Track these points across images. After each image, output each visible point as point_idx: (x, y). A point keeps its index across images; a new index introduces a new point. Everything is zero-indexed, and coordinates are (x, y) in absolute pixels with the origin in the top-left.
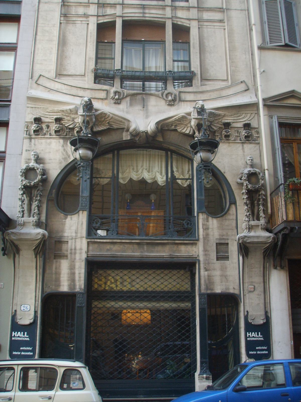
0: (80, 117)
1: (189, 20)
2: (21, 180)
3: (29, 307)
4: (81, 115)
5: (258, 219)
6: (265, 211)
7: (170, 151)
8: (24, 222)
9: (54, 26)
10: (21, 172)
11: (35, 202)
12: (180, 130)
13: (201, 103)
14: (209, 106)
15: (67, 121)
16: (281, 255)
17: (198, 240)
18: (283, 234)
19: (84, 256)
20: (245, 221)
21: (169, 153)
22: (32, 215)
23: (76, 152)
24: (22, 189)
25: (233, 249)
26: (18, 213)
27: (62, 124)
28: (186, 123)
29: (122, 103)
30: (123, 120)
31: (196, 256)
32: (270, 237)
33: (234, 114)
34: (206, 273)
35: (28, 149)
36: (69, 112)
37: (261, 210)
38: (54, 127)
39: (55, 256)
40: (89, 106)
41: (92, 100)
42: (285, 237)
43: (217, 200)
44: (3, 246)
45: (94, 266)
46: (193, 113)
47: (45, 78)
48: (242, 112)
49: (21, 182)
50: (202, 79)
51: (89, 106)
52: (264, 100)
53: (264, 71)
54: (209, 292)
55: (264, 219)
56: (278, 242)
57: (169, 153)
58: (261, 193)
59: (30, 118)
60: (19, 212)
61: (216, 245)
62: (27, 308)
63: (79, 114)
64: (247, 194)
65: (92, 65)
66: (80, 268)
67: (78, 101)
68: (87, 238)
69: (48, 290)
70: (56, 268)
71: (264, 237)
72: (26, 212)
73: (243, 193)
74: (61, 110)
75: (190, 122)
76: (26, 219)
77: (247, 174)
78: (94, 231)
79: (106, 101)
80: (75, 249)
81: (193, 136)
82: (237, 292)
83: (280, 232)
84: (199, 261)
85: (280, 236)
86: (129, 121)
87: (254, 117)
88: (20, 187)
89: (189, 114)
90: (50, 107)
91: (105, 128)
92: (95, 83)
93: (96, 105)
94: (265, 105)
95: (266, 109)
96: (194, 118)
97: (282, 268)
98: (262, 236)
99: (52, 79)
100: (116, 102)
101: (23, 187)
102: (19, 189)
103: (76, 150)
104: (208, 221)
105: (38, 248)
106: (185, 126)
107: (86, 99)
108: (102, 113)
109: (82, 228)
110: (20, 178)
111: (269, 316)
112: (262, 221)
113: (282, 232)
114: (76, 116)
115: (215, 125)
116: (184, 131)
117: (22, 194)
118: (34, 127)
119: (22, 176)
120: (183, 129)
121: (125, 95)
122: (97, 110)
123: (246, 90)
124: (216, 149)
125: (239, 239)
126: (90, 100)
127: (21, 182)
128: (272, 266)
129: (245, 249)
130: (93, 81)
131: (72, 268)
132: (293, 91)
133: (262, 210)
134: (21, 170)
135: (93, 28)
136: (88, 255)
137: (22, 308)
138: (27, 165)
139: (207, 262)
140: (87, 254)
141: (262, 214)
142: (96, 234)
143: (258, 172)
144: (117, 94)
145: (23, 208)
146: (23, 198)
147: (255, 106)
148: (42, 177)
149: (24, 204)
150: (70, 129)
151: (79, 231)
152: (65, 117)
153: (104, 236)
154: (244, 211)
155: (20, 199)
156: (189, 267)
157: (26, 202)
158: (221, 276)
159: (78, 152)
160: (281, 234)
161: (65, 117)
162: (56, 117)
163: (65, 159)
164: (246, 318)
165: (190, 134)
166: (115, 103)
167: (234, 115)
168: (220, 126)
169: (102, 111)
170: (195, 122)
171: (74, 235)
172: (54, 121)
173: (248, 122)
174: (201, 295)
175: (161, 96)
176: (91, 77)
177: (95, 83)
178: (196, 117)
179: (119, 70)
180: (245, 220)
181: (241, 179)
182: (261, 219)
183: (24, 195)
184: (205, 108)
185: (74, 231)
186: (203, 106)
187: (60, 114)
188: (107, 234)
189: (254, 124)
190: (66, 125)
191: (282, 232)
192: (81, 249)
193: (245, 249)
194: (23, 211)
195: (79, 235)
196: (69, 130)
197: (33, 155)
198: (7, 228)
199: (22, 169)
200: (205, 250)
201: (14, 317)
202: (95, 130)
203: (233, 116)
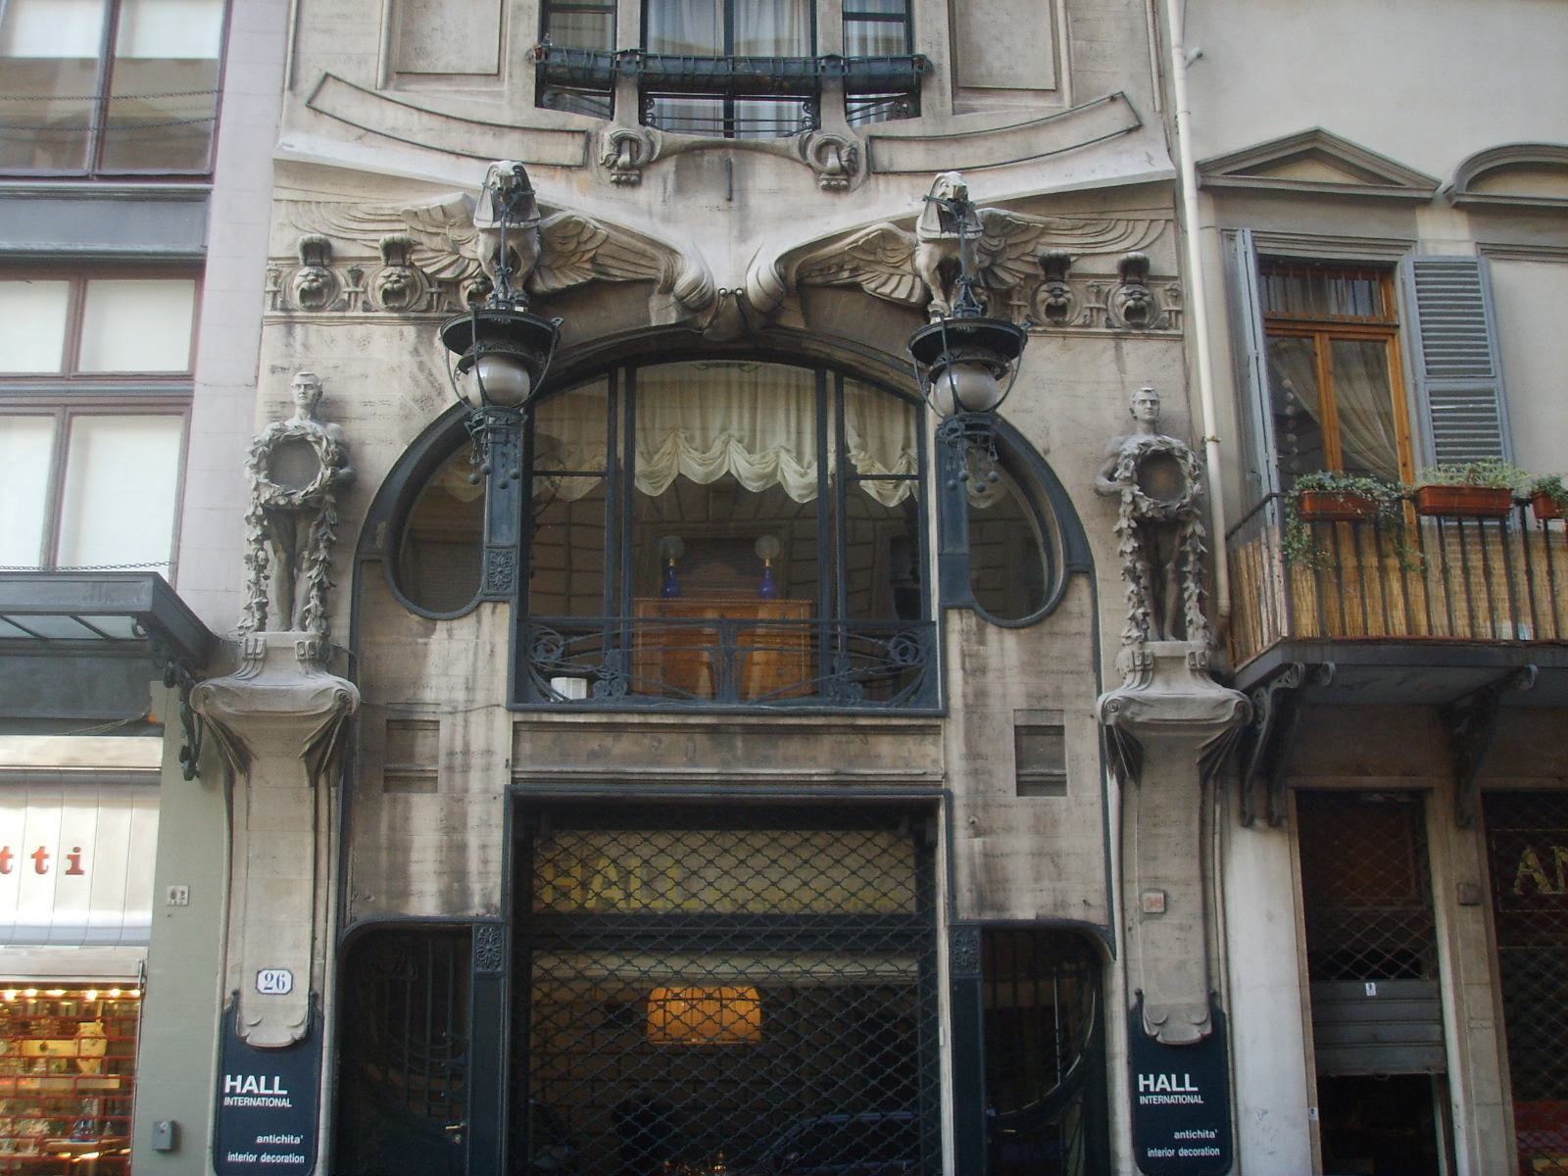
0: (482, 237)
2: (254, 484)
3: (287, 979)
4: (483, 230)
5: (1180, 633)
6: (1206, 603)
7: (832, 369)
8: (267, 650)
10: (253, 453)
11: (310, 569)
12: (873, 286)
13: (953, 179)
15: (430, 254)
16: (1271, 772)
17: (944, 715)
18: (1277, 692)
19: (501, 778)
20: (1129, 642)
21: (830, 376)
22: (296, 619)
23: (467, 373)
24: (260, 520)
25: (1083, 749)
26: (244, 614)
27: (412, 265)
29: (644, 182)
30: (648, 249)
31: (939, 778)
32: (1225, 703)
33: (1082, 223)
34: (978, 842)
36: (440, 217)
37: (1190, 596)
38: (380, 276)
39: (387, 779)
40: (515, 196)
41: (528, 170)
42: (1286, 701)
43: (1019, 560)
44: (185, 742)
45: (540, 819)
47: (343, 87)
49: (255, 494)
50: (957, 88)
51: (515, 196)
52: (1201, 168)
53: (1200, 56)
54: (989, 916)
55: (1201, 632)
56: (1256, 721)
57: (830, 376)
58: (1190, 530)
59: (287, 242)
60: (248, 608)
61: (1017, 734)
62: (281, 984)
63: (478, 225)
64: (1135, 533)
66: (486, 824)
67: (473, 177)
68: (511, 710)
69: (362, 913)
70: (392, 828)
71: (1203, 702)
72: (273, 608)
73: (1120, 532)
74: (406, 212)
76: (273, 634)
78: (540, 680)
79: (583, 175)
80: (466, 752)
81: (921, 311)
82: (1097, 917)
83: (1264, 682)
84: (949, 796)
85: (1267, 699)
86: (672, 252)
87: (1162, 234)
88: (250, 512)
89: (908, 224)
90: (363, 200)
92: (539, 103)
93: (546, 189)
94: (1203, 189)
95: (1209, 202)
96: (927, 241)
97: (1274, 823)
98: (1193, 701)
99: (374, 91)
101: (260, 511)
102: (248, 519)
103: (465, 366)
104: (982, 641)
105: (321, 750)
106: (891, 270)
107: (506, 167)
108: (567, 223)
109: (493, 672)
110: (250, 477)
111: (1225, 1010)
112: (1196, 642)
113: (1275, 685)
114: (466, 234)
115: (1010, 265)
116: (887, 290)
117: (259, 541)
118: (301, 277)
119: (256, 467)
120: (884, 284)
122: (546, 211)
123: (1129, 131)
124: (1015, 361)
125: (1105, 712)
126: (520, 171)
127: (255, 494)
128: (1234, 814)
129: (1128, 748)
130: (533, 99)
131: (454, 826)
132: (1315, 134)
133: (1195, 598)
134: (255, 444)
136: (517, 776)
137: (262, 984)
138: (276, 425)
139: (982, 802)
140: (513, 772)
141: (1193, 613)
142: (546, 694)
143: (1180, 450)
144: (626, 145)
145: (263, 593)
146: (261, 554)
147: (1164, 190)
148: (333, 474)
149: (267, 578)
150: (441, 283)
151: (481, 683)
152: (424, 239)
153: (579, 701)
154: (1125, 601)
155: (248, 559)
156: (909, 819)
157: (274, 570)
158: (1038, 854)
159: (473, 374)
160: (1270, 693)
161: (424, 239)
162: (388, 236)
163: (424, 401)
164: (1134, 1018)
166: (618, 183)
168: (1029, 270)
169: (569, 213)
171: (460, 696)
172: (381, 254)
173: (1140, 254)
174: (957, 929)
175: (796, 154)
176: (524, 80)
177: (539, 103)
178: (937, 235)
179: (634, 52)
180: (1129, 637)
181: (1111, 478)
182: (1190, 631)
183: (268, 545)
184: (971, 199)
185: (460, 683)
186: (961, 191)
187: (403, 226)
188: (590, 694)
189: (1162, 262)
190: (428, 270)
191: (1275, 685)
192: (489, 752)
193: (1128, 748)
194: (262, 606)
195: (480, 697)
196: (440, 290)
197: (299, 386)
198: (199, 673)
199: (259, 441)
200: (973, 754)
201: (229, 1019)
203: (1080, 232)
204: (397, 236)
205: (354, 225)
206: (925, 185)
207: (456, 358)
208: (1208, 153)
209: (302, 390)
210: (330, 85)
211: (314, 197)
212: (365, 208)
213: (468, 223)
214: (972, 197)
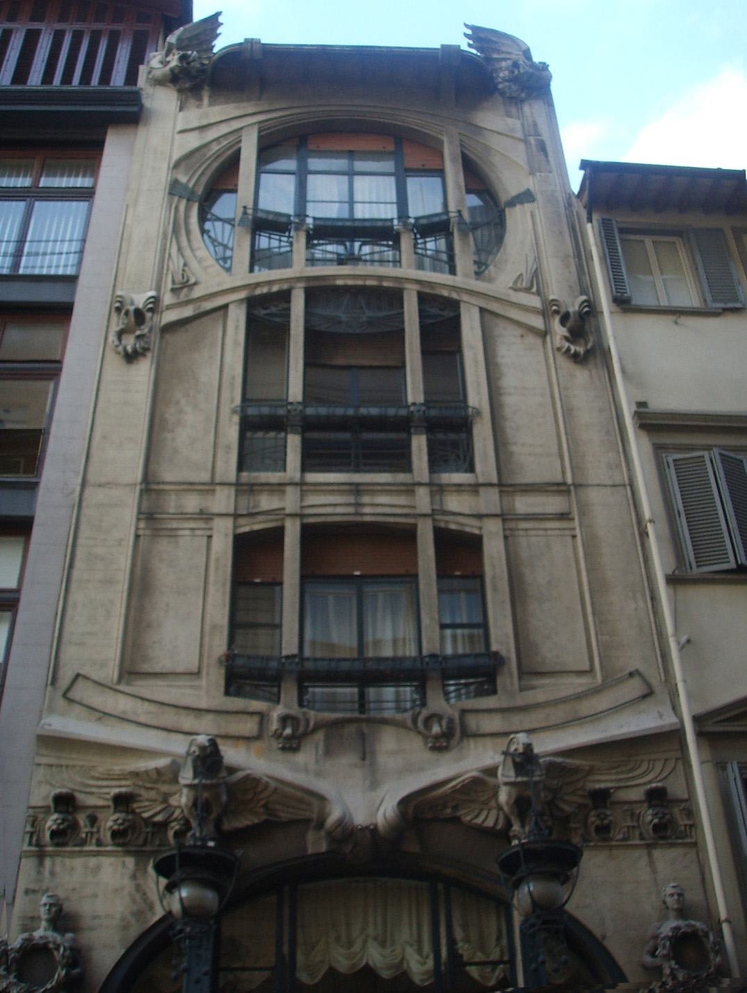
0: (185, 791)
1: (480, 517)
9: (120, 545)
12: (468, 818)
13: (522, 738)
14: (546, 745)
15: (147, 803)
21: (440, 886)
27: (133, 812)
28: (482, 799)
35: (31, 886)
38: (110, 821)
41: (219, 741)
46: (503, 769)
48: (653, 756)
52: (697, 719)
53: (688, 641)
59: (42, 795)
65: (219, 645)
67: (179, 746)
75: (495, 795)
77: (669, 938)
86: (322, 798)
87: (674, 769)
89: (491, 771)
91: (256, 821)
93: (232, 754)
94: (700, 735)
96: (506, 784)
100: (287, 745)
107: (202, 739)
108: (247, 778)
115: (567, 798)
116: (479, 820)
120: (477, 816)
121: (312, 724)
124: (575, 869)
126: (213, 743)
130: (222, 689)
135: (223, 546)
143: (703, 931)
144: (289, 722)
161: (143, 792)
162: (117, 790)
163: (139, 915)
165: (499, 827)
167: (619, 766)
168: (581, 801)
170: (509, 795)
176: (215, 677)
178: (512, 779)
179: (294, 656)
186: (528, 747)
189: (676, 789)
202: (227, 826)
204: (123, 790)
205: (92, 782)
206: (502, 743)
207: (163, 881)
208: (701, 709)
209: (47, 907)
210: (80, 682)
211: (64, 762)
212: (100, 769)
213: (175, 780)
214: (536, 750)
